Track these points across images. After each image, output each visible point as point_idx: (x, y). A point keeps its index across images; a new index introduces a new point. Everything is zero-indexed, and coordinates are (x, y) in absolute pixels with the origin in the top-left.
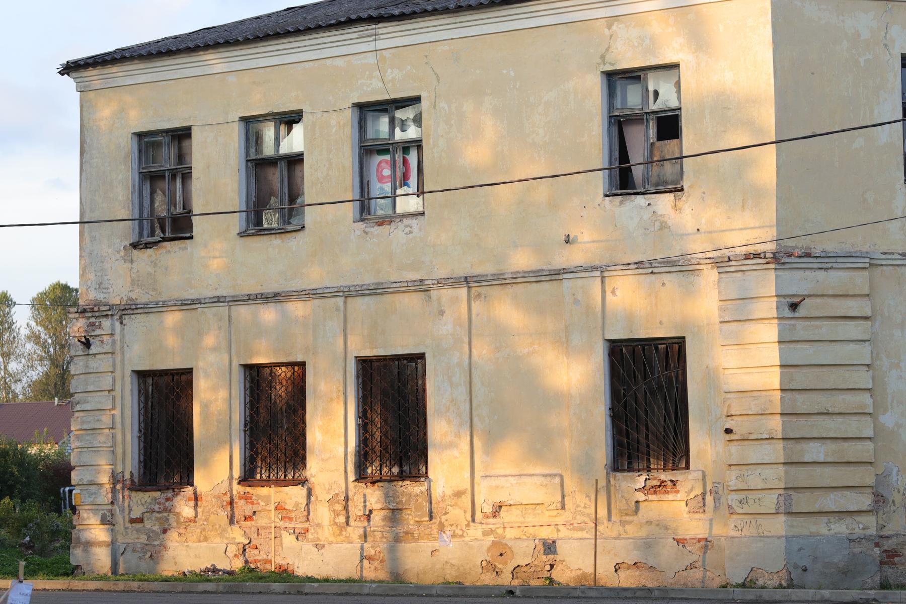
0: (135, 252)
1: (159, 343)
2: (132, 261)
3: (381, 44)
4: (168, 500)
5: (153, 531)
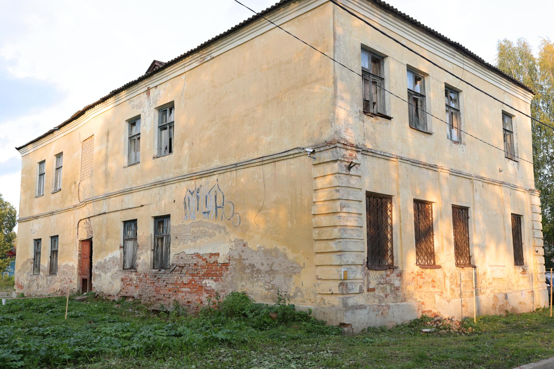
2: (363, 121)
4: (387, 276)
5: (381, 296)
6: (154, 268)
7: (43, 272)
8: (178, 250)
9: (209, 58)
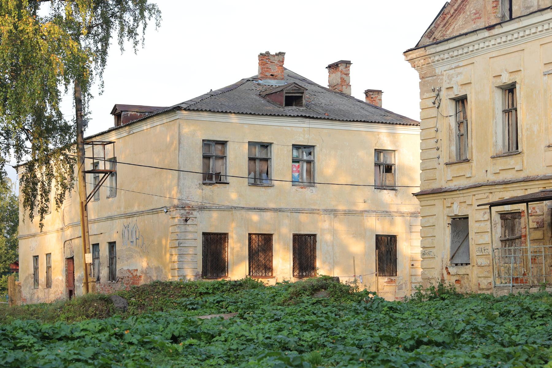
0: (204, 186)
1: (212, 223)
2: (202, 190)
3: (311, 126)
6: (109, 280)
7: (41, 285)
8: (121, 267)
9: (132, 133)
